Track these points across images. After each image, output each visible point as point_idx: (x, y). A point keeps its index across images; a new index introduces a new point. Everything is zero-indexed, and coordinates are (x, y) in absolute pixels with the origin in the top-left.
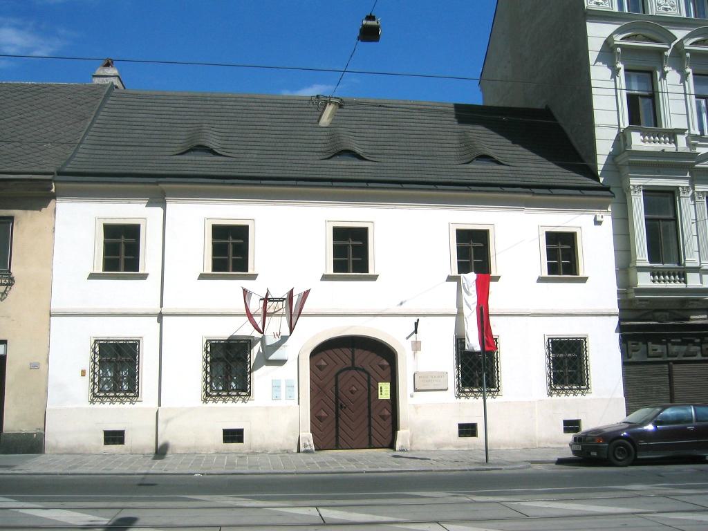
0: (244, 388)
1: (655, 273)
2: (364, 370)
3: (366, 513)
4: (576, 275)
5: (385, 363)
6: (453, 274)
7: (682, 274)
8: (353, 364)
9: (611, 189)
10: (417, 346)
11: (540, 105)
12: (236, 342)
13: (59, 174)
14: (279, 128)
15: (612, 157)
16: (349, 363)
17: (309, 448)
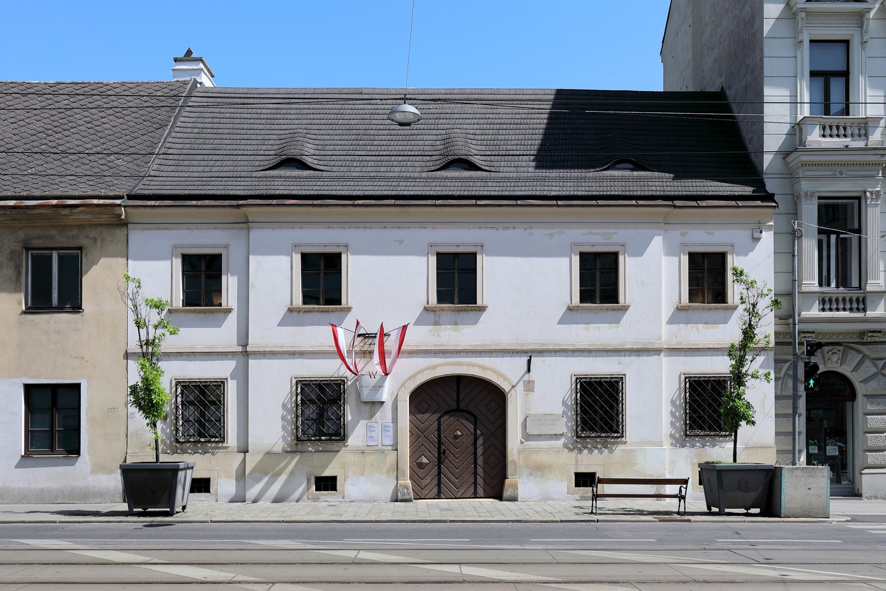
0: (339, 435)
1: (826, 303)
2: (470, 413)
3: (397, 555)
4: (725, 303)
5: (762, 404)
7: (861, 304)
9: (776, 198)
11: (713, 87)
13: (131, 197)
15: (785, 154)
16: (454, 406)
17: (408, 497)
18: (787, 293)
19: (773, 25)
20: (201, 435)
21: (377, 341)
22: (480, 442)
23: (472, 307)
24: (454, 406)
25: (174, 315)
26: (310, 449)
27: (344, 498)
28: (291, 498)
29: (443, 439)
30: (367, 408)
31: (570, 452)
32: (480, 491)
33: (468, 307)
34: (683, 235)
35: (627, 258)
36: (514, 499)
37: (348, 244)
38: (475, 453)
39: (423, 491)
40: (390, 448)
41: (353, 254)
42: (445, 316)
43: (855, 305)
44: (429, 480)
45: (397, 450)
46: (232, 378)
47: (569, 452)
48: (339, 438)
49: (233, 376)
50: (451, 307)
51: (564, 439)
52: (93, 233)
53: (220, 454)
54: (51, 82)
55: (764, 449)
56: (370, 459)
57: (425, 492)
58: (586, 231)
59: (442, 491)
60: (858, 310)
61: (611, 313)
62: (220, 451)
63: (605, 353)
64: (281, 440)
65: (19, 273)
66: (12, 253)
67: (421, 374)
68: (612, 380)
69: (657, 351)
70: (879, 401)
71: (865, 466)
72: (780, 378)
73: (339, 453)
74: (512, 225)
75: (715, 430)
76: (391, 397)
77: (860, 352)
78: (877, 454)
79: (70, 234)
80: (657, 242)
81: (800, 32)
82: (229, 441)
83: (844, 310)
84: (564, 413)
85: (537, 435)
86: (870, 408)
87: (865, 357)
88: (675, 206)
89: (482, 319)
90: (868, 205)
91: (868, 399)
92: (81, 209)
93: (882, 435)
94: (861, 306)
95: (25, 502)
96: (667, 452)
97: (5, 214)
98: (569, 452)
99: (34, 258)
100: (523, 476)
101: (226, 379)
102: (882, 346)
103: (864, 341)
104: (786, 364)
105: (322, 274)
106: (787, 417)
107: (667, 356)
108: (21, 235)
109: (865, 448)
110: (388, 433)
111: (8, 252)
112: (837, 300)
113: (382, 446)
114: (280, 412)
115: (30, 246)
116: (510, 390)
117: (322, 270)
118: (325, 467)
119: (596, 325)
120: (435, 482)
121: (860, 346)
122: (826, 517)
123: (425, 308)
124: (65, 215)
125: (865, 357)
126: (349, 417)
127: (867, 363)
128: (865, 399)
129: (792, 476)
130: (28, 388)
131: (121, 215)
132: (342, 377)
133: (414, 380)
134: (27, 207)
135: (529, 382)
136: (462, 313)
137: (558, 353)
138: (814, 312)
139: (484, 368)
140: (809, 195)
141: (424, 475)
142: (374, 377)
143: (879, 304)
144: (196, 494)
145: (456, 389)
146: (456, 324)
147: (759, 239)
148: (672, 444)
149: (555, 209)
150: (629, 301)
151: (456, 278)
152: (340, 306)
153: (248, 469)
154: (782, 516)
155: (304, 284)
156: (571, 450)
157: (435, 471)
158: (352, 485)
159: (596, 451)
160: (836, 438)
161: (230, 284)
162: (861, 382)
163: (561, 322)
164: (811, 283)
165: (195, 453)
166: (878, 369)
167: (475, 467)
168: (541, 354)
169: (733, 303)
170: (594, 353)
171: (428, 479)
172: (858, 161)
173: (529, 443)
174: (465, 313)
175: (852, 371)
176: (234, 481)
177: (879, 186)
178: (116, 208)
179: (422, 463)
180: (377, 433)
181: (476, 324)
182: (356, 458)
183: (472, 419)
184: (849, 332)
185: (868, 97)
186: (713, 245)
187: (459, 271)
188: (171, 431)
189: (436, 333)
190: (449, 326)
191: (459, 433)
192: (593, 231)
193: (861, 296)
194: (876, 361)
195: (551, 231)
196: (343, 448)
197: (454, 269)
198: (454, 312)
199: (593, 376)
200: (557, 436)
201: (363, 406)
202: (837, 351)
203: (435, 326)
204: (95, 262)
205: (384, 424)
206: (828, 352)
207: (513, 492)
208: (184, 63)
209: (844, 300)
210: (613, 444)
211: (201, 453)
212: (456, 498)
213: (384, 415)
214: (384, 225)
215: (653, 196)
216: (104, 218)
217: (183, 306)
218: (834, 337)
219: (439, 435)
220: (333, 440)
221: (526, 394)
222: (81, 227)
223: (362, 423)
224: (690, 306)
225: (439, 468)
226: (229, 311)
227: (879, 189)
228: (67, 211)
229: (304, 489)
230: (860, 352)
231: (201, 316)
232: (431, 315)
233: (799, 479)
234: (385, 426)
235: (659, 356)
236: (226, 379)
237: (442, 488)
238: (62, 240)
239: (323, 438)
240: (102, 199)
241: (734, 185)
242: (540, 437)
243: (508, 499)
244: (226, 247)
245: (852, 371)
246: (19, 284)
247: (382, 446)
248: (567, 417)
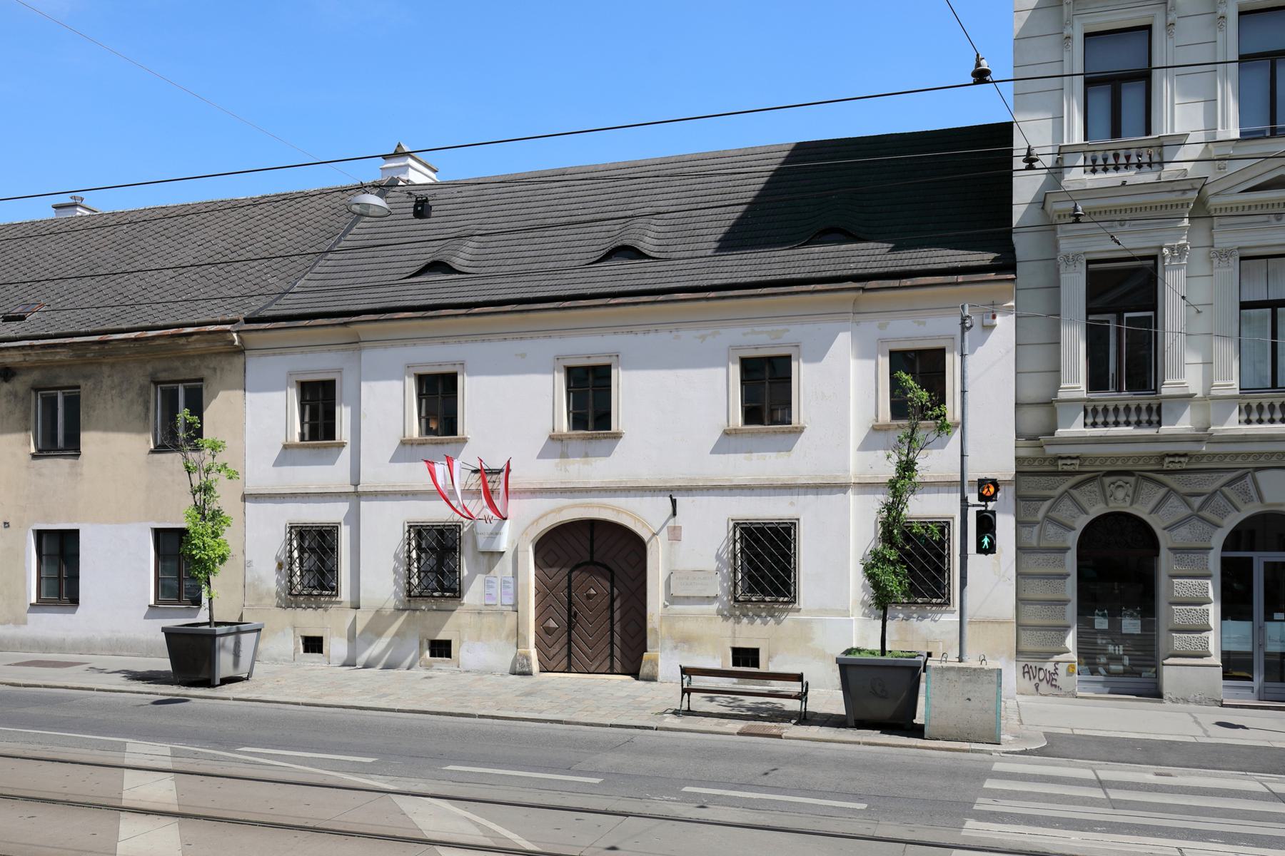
1: (1094, 414)
5: (996, 562)
6: (881, 421)
7: (1154, 415)
8: (592, 557)
13: (248, 321)
16: (588, 559)
17: (527, 670)
18: (1045, 401)
19: (1027, 20)
20: (323, 588)
21: (502, 475)
22: (617, 604)
23: (604, 434)
24: (588, 559)
25: (289, 450)
26: (423, 608)
27: (458, 667)
28: (402, 665)
29: (575, 598)
30: (484, 560)
31: (725, 622)
32: (618, 665)
33: (599, 434)
34: (881, 327)
35: (802, 365)
36: (652, 678)
37: (955, 335)
38: (612, 618)
39: (551, 662)
40: (511, 608)
41: (470, 375)
42: (576, 446)
43: (1144, 417)
44: (558, 649)
45: (517, 611)
46: (345, 524)
47: (723, 621)
49: (346, 519)
50: (579, 435)
51: (718, 604)
52: (213, 363)
53: (333, 610)
54: (257, 196)
55: (996, 625)
56: (488, 620)
57: (553, 663)
58: (748, 330)
59: (573, 663)
60: (1150, 423)
61: (780, 437)
62: (334, 606)
63: (772, 491)
64: (393, 597)
65: (148, 409)
66: (142, 388)
67: (545, 518)
69: (843, 488)
70: (1193, 558)
71: (1171, 652)
72: (1038, 523)
73: (454, 613)
74: (653, 328)
76: (512, 546)
77: (1162, 484)
78: (1190, 635)
79: (192, 364)
80: (844, 341)
81: (1066, 24)
82: (343, 595)
83: (1128, 423)
84: (718, 569)
85: (684, 597)
86: (1177, 569)
87: (1172, 492)
88: (864, 290)
89: (617, 448)
90: (1167, 268)
91: (1175, 554)
92: (195, 337)
93: (1198, 608)
94: (1155, 418)
95: (152, 655)
96: (855, 625)
97: (130, 347)
98: (723, 621)
99: (163, 391)
100: (665, 649)
101: (340, 523)
102: (1198, 475)
103: (1165, 468)
104: (1045, 503)
105: (440, 398)
106: (1046, 579)
107: (858, 494)
108: (149, 368)
109: (1171, 626)
110: (508, 590)
111: (138, 387)
112: (1116, 409)
113: (502, 605)
114: (392, 563)
115: (157, 380)
116: (650, 539)
117: (440, 393)
118: (438, 629)
119: (759, 454)
120: (565, 652)
121: (1162, 475)
122: (994, 742)
123: (550, 436)
124: (183, 345)
125: (1171, 491)
126: (465, 572)
127: (1174, 501)
128: (1171, 554)
129: (942, 680)
130: (158, 533)
131: (234, 341)
132: (457, 522)
134: (147, 339)
135: (675, 528)
136: (593, 441)
137: (711, 491)
138: (1075, 428)
139: (618, 511)
140: (1072, 259)
141: (552, 643)
143: (1182, 414)
144: (310, 654)
145: (589, 536)
146: (586, 455)
147: (993, 327)
148: (864, 614)
149: (703, 304)
151: (591, 398)
152: (455, 437)
153: (358, 632)
154: (925, 737)
156: (726, 618)
157: (564, 639)
158: (468, 651)
159: (758, 621)
160: (1138, 608)
161: (343, 415)
162: (1165, 529)
163: (715, 451)
164: (1075, 383)
165: (309, 608)
166: (1192, 509)
167: (612, 636)
168: (690, 493)
169: (954, 419)
170: (758, 491)
171: (557, 648)
172: (1147, 203)
173: (675, 607)
174: (597, 441)
175: (1151, 513)
176: (346, 641)
177: (1185, 237)
178: (228, 334)
179: (549, 628)
180: (496, 590)
181: (609, 456)
182: (472, 620)
183: (609, 574)
184: (1143, 455)
185: (1176, 107)
186: (924, 339)
187: (324, 402)
188: (286, 584)
189: (563, 469)
190: (578, 459)
191: (593, 592)
192: (756, 329)
193: (1154, 404)
194: (1188, 498)
195: (703, 332)
196: (459, 607)
197: (588, 387)
198: (584, 441)
199: (781, 521)
200: (709, 600)
201: (481, 556)
202: (1123, 484)
203: (563, 460)
204: (214, 396)
206: (1109, 486)
207: (651, 669)
208: (393, 160)
209: (1127, 409)
210: (782, 611)
211: (304, 608)
212: (589, 673)
213: (503, 568)
214: (504, 336)
215: (736, 284)
216: (219, 346)
218: (1119, 463)
219: (570, 593)
221: (672, 544)
222: (202, 357)
223: (480, 579)
225: (570, 635)
226: (342, 445)
227: (1185, 242)
228: (183, 341)
229: (415, 655)
230: (1162, 484)
231: (315, 451)
232: (558, 444)
233: (953, 685)
234: (505, 582)
235: (845, 494)
236: (340, 523)
237: (572, 661)
238: (185, 373)
239: (448, 594)
240: (219, 325)
241: (971, 252)
242: (687, 600)
243: (645, 678)
244: (340, 371)
245: (1151, 513)
246: (147, 421)
247: (502, 605)
248: (722, 575)
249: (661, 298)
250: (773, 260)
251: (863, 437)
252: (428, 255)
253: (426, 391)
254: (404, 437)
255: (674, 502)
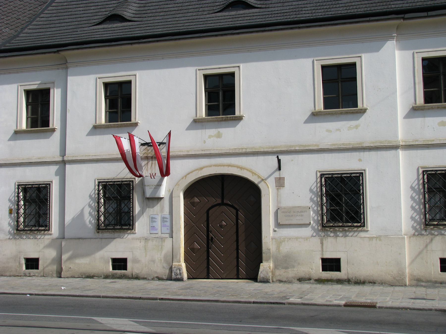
10: (280, 183)
12: (349, 175)
14: (81, 6)
17: (180, 277)
23: (232, 117)
33: (227, 117)
45: (172, 238)
48: (359, 224)
68: (107, 184)
69: (395, 147)
75: (339, 222)
110: (166, 223)
133: (185, 179)
135: (280, 178)
139: (242, 168)
142: (154, 178)
150: (366, 105)
155: (325, 92)
169: (363, 107)
191: (224, 223)
205: (164, 216)
212: (214, 279)
217: (205, 116)
220: (354, 226)
224: (424, 106)
226: (53, 130)
234: (164, 218)
237: (210, 271)
249: (267, 28)
250: (338, 6)
251: (406, 113)
252: (107, 13)
253: (110, 94)
254: (416, 104)
255: (279, 161)
